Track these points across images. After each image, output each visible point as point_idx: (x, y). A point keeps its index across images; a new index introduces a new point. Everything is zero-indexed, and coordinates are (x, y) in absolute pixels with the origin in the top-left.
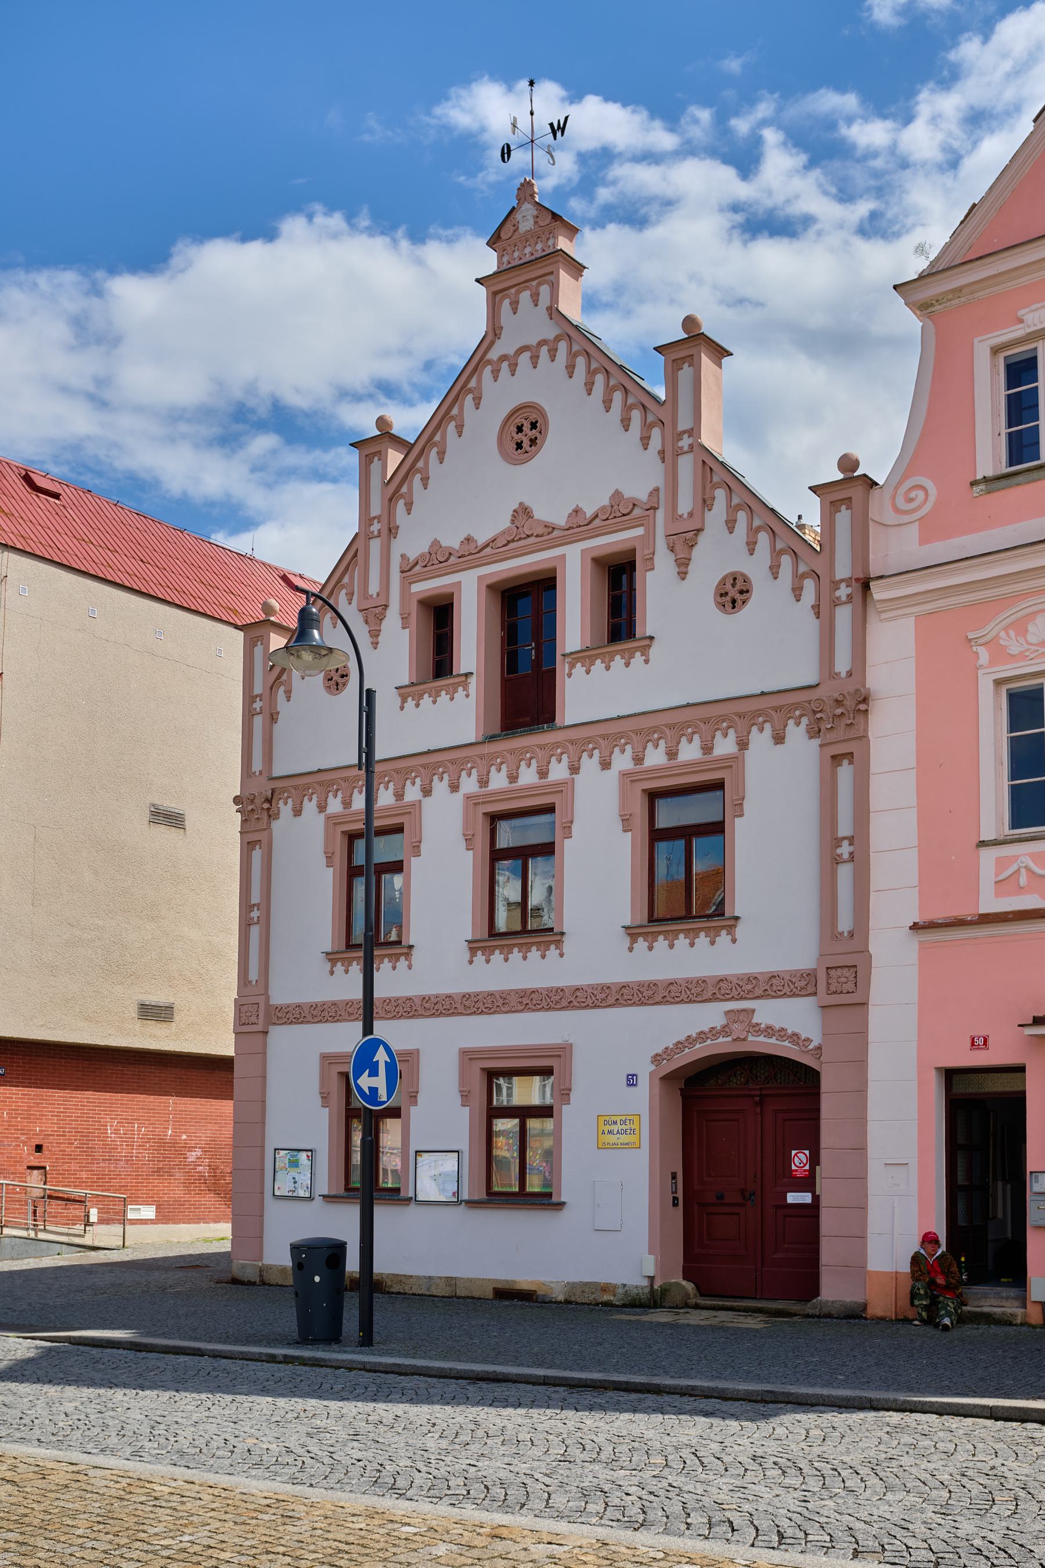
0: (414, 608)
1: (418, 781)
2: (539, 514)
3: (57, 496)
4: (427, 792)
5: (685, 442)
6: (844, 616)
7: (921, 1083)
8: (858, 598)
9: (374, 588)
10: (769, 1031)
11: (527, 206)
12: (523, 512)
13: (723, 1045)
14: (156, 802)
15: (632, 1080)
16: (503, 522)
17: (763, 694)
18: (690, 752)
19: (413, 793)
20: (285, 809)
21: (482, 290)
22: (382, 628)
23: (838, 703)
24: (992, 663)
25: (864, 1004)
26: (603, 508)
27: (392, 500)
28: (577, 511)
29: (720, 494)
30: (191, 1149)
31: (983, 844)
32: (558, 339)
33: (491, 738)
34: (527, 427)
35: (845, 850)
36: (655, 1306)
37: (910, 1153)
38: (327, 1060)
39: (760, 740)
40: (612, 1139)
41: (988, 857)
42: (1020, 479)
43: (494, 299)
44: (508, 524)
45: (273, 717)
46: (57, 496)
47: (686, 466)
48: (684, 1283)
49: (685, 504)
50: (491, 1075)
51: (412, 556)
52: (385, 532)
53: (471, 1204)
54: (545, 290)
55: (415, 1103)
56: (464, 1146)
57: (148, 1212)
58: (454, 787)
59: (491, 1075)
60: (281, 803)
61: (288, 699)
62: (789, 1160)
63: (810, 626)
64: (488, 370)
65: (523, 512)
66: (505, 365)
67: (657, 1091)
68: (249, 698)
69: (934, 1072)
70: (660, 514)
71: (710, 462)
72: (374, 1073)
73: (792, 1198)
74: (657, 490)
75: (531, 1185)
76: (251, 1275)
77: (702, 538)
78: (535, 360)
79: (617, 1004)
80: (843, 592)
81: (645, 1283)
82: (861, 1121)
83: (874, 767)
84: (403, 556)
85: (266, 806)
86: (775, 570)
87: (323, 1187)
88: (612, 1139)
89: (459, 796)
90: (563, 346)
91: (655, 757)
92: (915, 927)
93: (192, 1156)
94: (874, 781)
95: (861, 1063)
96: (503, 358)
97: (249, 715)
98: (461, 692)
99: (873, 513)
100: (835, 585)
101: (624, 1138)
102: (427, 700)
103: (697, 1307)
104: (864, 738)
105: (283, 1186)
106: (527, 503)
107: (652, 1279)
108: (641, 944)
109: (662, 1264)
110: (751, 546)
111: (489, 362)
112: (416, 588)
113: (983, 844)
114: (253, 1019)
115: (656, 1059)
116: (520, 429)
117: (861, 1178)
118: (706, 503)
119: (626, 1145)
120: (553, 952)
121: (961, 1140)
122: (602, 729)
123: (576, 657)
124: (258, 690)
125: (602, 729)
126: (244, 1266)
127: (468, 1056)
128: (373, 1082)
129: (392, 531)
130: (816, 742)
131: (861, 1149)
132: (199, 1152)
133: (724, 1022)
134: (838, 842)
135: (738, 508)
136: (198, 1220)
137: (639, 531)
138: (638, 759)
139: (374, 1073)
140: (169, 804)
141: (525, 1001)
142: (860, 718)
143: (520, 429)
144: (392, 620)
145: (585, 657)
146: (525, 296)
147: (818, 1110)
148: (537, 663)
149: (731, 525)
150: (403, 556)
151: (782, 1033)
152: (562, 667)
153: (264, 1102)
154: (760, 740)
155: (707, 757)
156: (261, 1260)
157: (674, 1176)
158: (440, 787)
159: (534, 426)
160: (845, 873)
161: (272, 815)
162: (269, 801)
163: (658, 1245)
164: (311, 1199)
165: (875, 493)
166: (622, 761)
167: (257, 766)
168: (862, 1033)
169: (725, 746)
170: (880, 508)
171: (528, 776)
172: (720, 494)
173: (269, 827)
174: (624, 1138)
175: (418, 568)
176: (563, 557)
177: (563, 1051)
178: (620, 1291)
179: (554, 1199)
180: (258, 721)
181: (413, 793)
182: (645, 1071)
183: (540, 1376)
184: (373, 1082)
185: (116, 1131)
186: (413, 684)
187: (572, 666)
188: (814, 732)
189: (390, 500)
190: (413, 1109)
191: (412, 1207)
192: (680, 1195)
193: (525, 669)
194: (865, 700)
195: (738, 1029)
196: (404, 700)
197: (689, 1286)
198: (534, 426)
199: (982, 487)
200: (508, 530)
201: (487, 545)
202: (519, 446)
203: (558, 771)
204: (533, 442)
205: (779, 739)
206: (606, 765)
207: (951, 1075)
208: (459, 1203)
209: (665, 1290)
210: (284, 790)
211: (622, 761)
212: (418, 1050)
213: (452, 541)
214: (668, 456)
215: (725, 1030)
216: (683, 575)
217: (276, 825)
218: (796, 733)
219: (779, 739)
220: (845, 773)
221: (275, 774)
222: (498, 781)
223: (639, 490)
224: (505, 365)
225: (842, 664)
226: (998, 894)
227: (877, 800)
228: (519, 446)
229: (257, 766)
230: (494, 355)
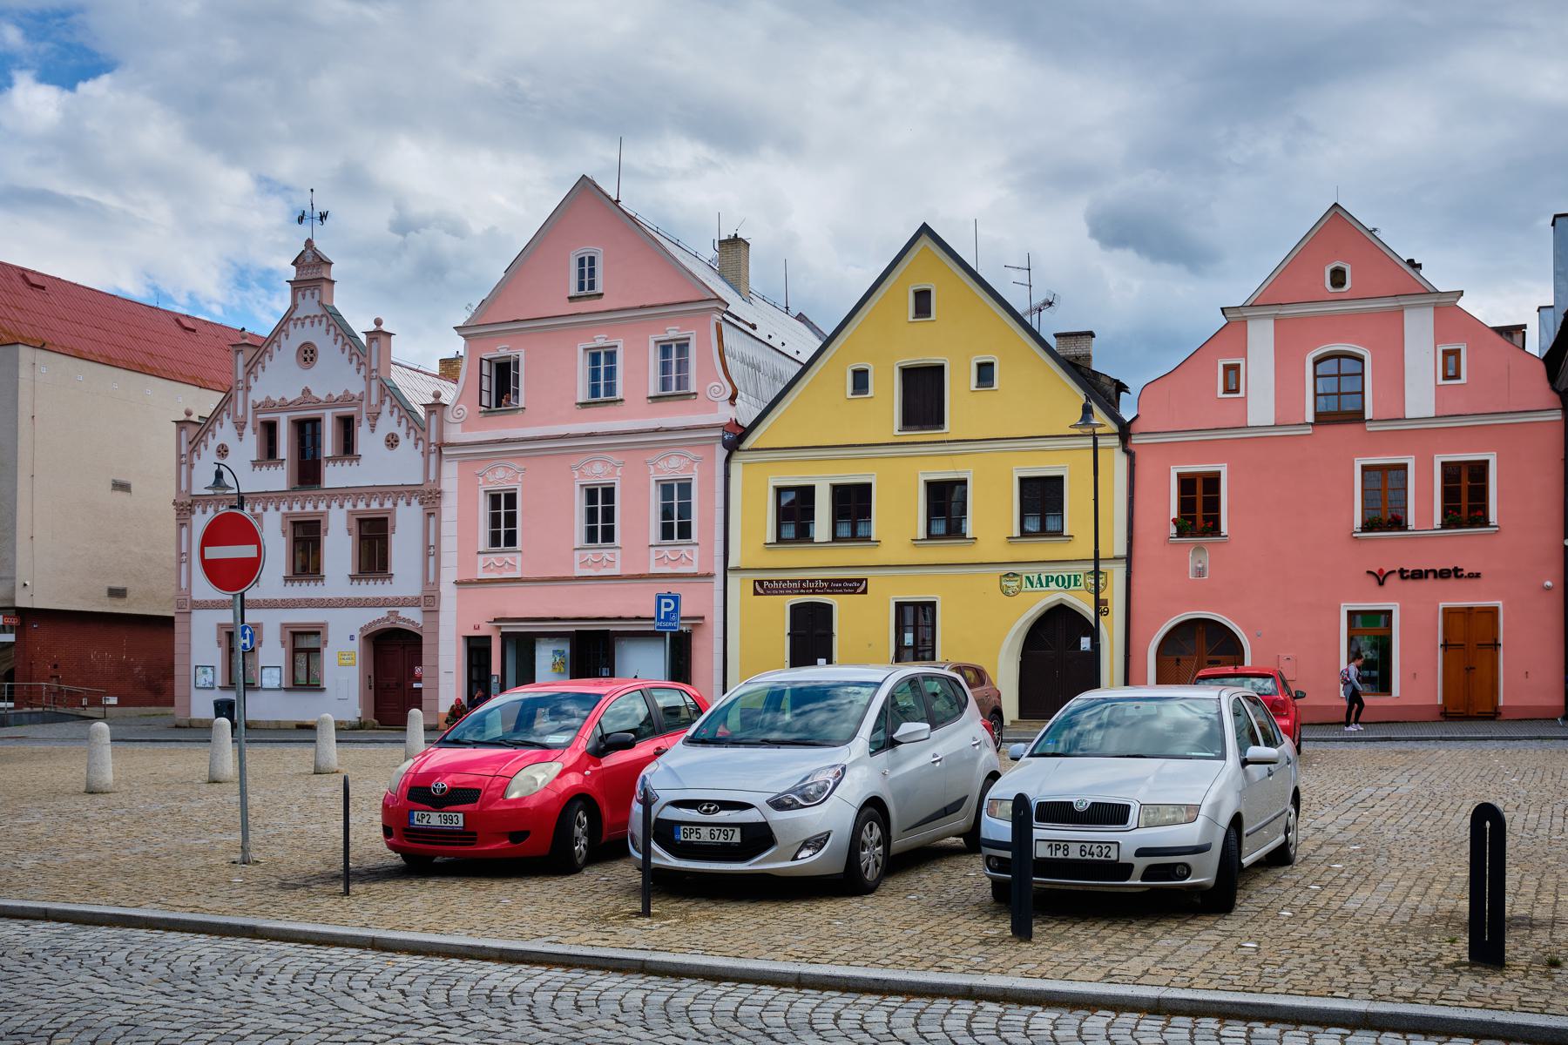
0: (259, 425)
1: (261, 504)
2: (314, 393)
3: (43, 288)
4: (265, 509)
5: (374, 374)
6: (433, 458)
7: (457, 642)
8: (437, 451)
9: (240, 413)
10: (404, 620)
11: (309, 251)
12: (307, 391)
13: (387, 625)
14: (115, 478)
15: (352, 638)
16: (299, 395)
17: (403, 485)
18: (375, 505)
19: (258, 509)
20: (198, 510)
21: (289, 285)
22: (244, 432)
23: (430, 493)
24: (484, 483)
25: (437, 611)
26: (341, 396)
27: (249, 373)
28: (330, 395)
29: (388, 399)
30: (136, 666)
31: (479, 553)
32: (322, 316)
33: (294, 489)
34: (309, 352)
35: (432, 550)
36: (362, 729)
37: (453, 669)
38: (221, 626)
39: (402, 503)
40: (344, 661)
41: (481, 557)
42: (496, 413)
43: (295, 291)
44: (301, 396)
45: (192, 466)
46: (43, 288)
47: (375, 384)
48: (373, 720)
49: (374, 401)
50: (294, 634)
51: (258, 402)
52: (244, 388)
53: (286, 689)
54: (317, 292)
55: (261, 646)
56: (283, 665)
57: (113, 701)
58: (277, 509)
59: (294, 634)
60: (196, 507)
61: (199, 458)
62: (414, 670)
63: (420, 460)
64: (292, 322)
65: (307, 391)
66: (299, 322)
67: (362, 642)
68: (180, 456)
69: (461, 639)
70: (364, 403)
71: (383, 385)
72: (245, 638)
73: (415, 685)
74: (363, 392)
75: (300, 679)
76: (185, 723)
77: (381, 417)
78: (312, 323)
79: (346, 606)
80: (433, 448)
81: (358, 720)
82: (437, 656)
83: (443, 519)
84: (253, 401)
85: (189, 508)
86: (408, 435)
87: (219, 683)
88: (344, 661)
89: (279, 514)
90: (324, 319)
91: (361, 506)
92: (456, 583)
93: (137, 670)
94: (442, 524)
95: (437, 633)
96: (299, 319)
97: (179, 464)
98: (280, 467)
99: (445, 417)
100: (430, 445)
101: (349, 661)
102: (264, 468)
103: (378, 729)
104: (439, 508)
105: (201, 683)
106: (309, 387)
107: (360, 718)
108: (356, 582)
109: (364, 712)
110: (399, 424)
111: (292, 319)
112: (259, 416)
113: (479, 553)
114: (184, 606)
115: (362, 629)
116: (306, 352)
117: (437, 677)
118: (382, 402)
119: (350, 665)
120: (320, 583)
121: (474, 662)
122: (340, 491)
123: (328, 459)
124: (183, 452)
125: (340, 491)
126: (181, 719)
127: (285, 626)
128: (245, 641)
129: (248, 388)
130: (422, 507)
131: (437, 666)
132: (140, 668)
133: (387, 615)
134: (429, 547)
135: (394, 406)
136: (140, 705)
137: (355, 409)
138: (355, 506)
139: (245, 638)
140: (122, 479)
141: (308, 603)
142: (438, 500)
143: (306, 352)
144: (248, 431)
145: (333, 459)
146: (308, 293)
147: (421, 651)
148: (314, 455)
149: (392, 413)
150: (253, 401)
151: (408, 621)
152: (323, 463)
153: (190, 645)
154: (402, 503)
155: (381, 508)
156: (189, 716)
157: (370, 677)
158: (271, 508)
159: (312, 352)
160: (432, 559)
161: (192, 512)
162: (190, 505)
163: (363, 704)
164: (213, 688)
165: (446, 408)
166: (348, 506)
167: (184, 487)
168: (437, 622)
169: (388, 505)
170: (449, 416)
171: (309, 508)
172: (388, 399)
173: (190, 519)
174: (349, 661)
175: (260, 408)
176: (324, 414)
177: (323, 626)
178: (348, 724)
179: (321, 687)
180: (184, 468)
181: (258, 509)
182: (357, 634)
183: (367, 938)
184: (245, 641)
185: (95, 656)
186: (258, 461)
187: (328, 462)
188: (421, 503)
189: (247, 374)
190: (260, 648)
191: (261, 693)
192: (373, 685)
193: (309, 458)
194: (439, 493)
195: (392, 619)
196: (254, 467)
197: (376, 721)
198: (312, 352)
199: (483, 414)
200: (301, 398)
201: (291, 403)
202: (306, 360)
203: (322, 507)
204: (312, 359)
205: (409, 504)
206: (341, 506)
207: (469, 639)
208: (280, 689)
209: (365, 723)
210: (198, 501)
211: (348, 506)
212: (262, 623)
213: (277, 399)
214: (368, 379)
215: (388, 619)
216: (373, 431)
217: (193, 517)
218: (415, 502)
219: (409, 504)
220: (432, 520)
221: (194, 493)
222: (297, 508)
223: (355, 391)
224: (299, 322)
225: (432, 477)
226: (484, 572)
227: (444, 532)
228: (306, 360)
229: (184, 487)
230: (295, 316)
